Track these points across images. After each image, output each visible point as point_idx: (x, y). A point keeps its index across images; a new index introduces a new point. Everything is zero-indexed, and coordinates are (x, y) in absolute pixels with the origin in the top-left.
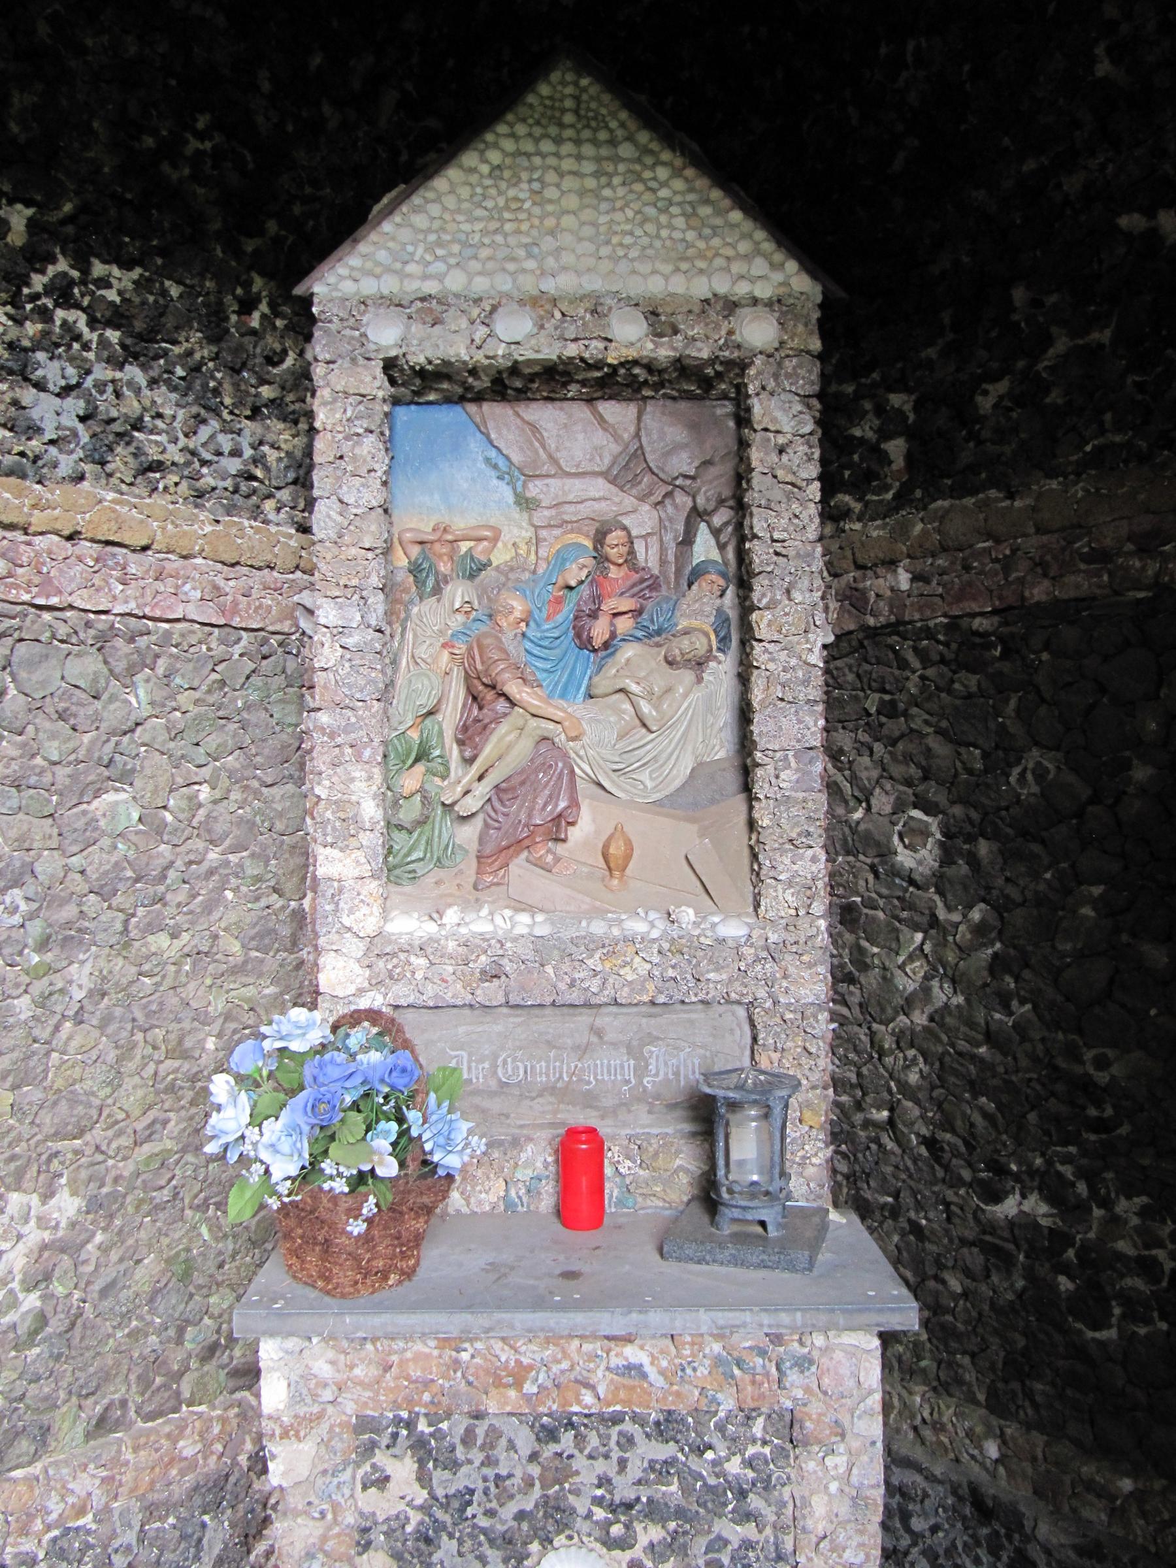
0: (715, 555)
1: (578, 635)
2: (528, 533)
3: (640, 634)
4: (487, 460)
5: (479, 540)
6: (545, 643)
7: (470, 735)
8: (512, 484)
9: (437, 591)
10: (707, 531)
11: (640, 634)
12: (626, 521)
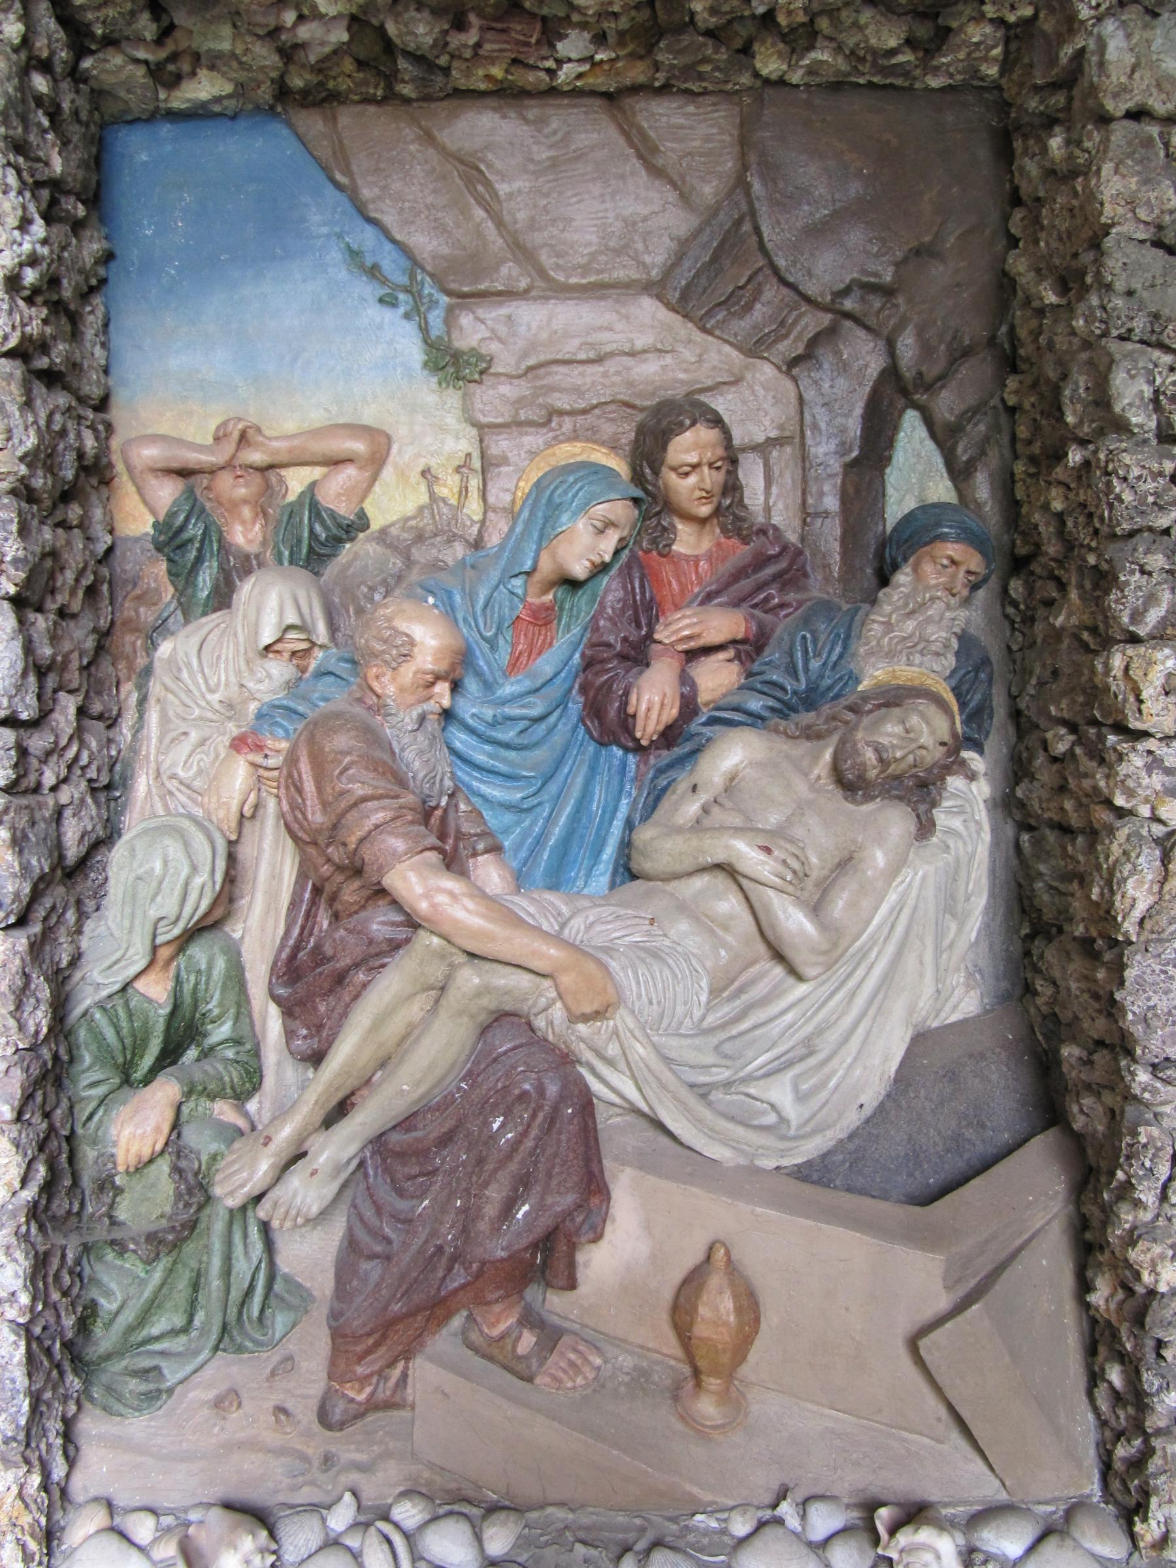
0: (942, 490)
1: (594, 710)
2: (462, 443)
3: (756, 704)
4: (354, 255)
5: (335, 462)
6: (508, 734)
7: (314, 983)
8: (417, 313)
9: (222, 598)
10: (922, 432)
11: (756, 704)
12: (720, 404)
